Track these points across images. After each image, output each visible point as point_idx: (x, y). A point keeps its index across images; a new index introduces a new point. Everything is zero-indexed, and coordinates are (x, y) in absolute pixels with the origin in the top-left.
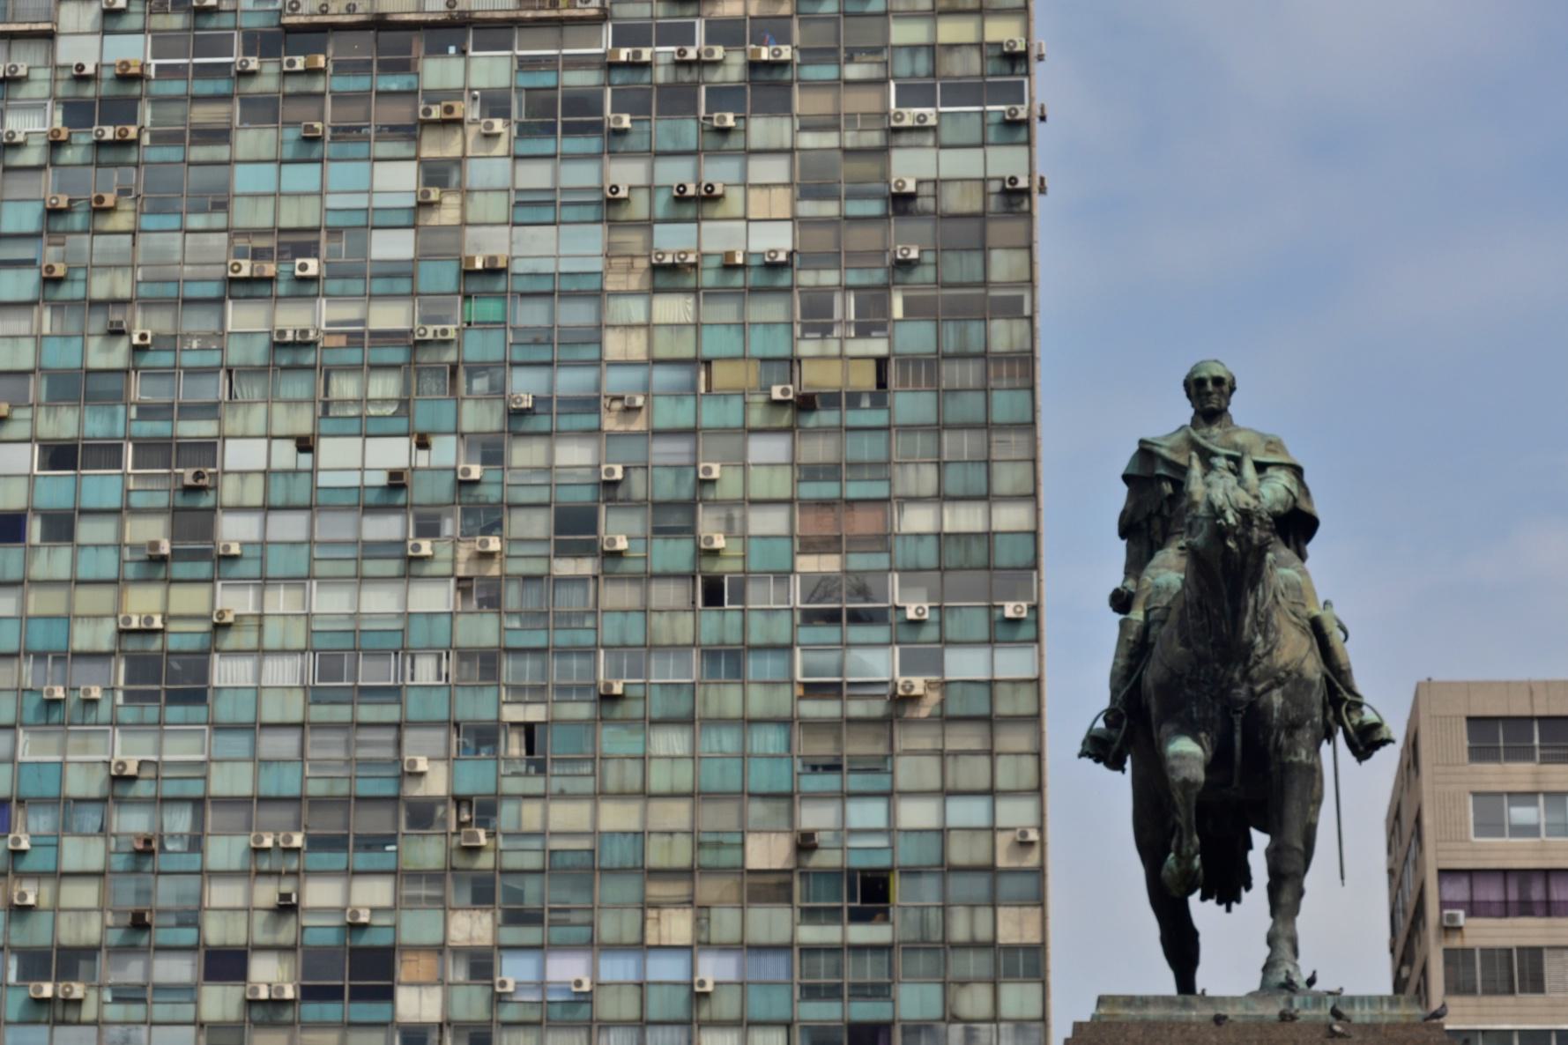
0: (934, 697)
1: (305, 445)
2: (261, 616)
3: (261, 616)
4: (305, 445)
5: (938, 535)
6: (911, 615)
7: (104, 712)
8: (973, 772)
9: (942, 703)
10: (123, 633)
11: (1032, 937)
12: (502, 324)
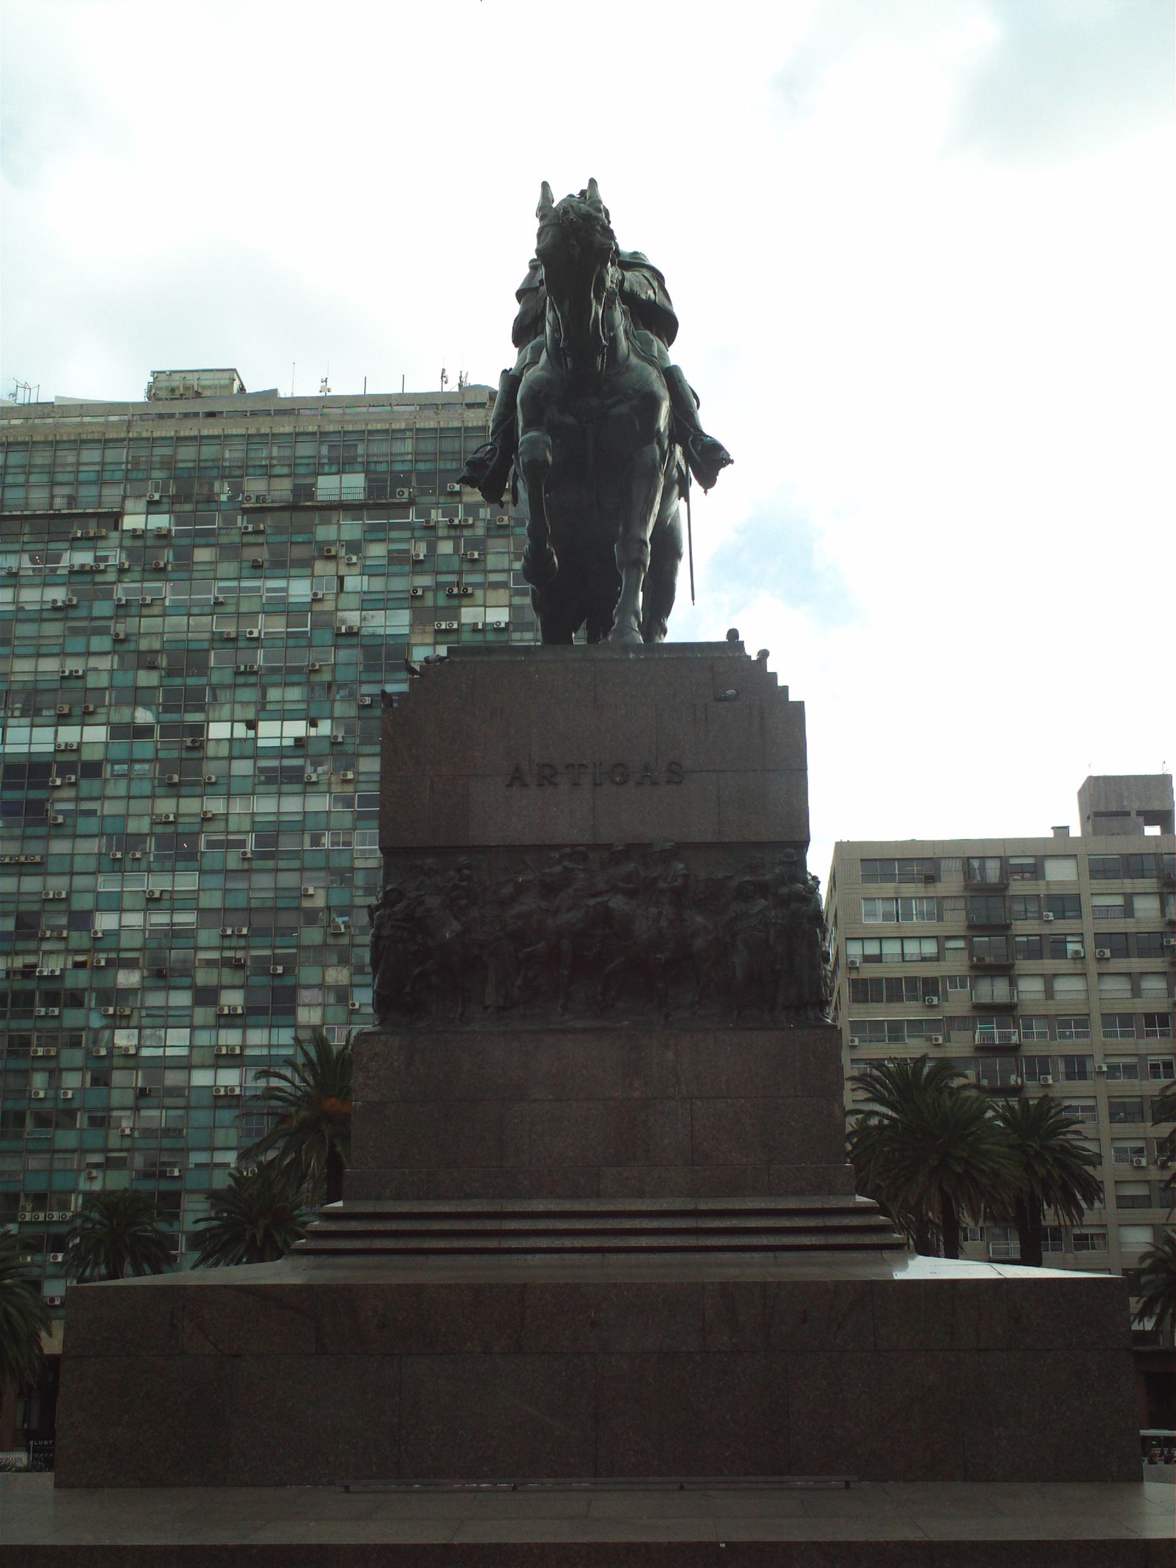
1: (251, 725)
4: (251, 725)
7: (144, 865)
12: (22, 1224)
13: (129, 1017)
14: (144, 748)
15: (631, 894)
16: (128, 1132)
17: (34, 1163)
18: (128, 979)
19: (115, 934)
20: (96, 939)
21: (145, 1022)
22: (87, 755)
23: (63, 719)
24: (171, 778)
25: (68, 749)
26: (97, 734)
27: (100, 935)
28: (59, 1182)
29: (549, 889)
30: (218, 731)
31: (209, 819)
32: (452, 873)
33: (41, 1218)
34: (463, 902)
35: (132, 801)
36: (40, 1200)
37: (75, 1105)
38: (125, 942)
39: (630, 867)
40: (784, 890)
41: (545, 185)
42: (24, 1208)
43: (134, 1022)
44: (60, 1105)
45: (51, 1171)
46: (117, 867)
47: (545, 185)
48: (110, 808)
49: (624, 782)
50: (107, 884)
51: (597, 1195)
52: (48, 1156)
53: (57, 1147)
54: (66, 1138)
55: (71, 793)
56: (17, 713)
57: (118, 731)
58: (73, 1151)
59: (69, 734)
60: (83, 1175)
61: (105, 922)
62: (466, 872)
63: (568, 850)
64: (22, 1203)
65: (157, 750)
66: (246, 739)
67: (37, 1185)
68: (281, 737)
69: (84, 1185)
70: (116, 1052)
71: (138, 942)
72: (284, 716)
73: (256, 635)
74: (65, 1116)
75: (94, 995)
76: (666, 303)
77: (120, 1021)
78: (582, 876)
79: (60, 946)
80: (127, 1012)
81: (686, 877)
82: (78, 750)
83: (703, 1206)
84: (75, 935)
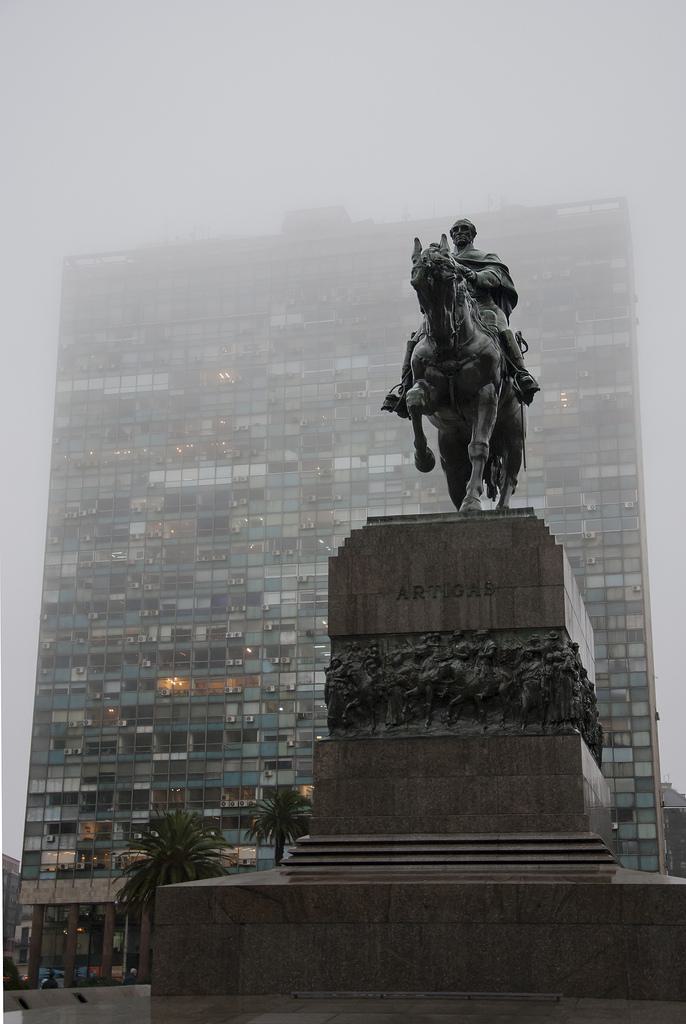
0: (600, 538)
1: (364, 458)
2: (350, 521)
3: (350, 521)
4: (364, 458)
5: (598, 478)
6: (589, 508)
7: (295, 558)
8: (616, 566)
9: (603, 541)
10: (301, 530)
11: (648, 773)
12: (223, 809)
13: (289, 664)
14: (291, 478)
15: (464, 659)
16: (291, 744)
17: (231, 766)
18: (288, 638)
19: (278, 607)
20: (265, 611)
21: (300, 667)
22: (254, 484)
23: (236, 460)
24: (311, 498)
25: (241, 481)
26: (260, 469)
27: (267, 608)
28: (248, 780)
29: (419, 658)
30: (341, 464)
31: (339, 525)
32: (367, 649)
33: (236, 805)
34: (372, 666)
35: (286, 515)
36: (235, 792)
37: (256, 726)
38: (285, 613)
39: (462, 644)
40: (549, 655)
41: (417, 240)
42: (224, 798)
43: (293, 668)
44: (245, 727)
45: (241, 772)
46: (277, 560)
47: (417, 240)
48: (274, 520)
49: (461, 595)
50: (272, 573)
51: (446, 832)
52: (239, 761)
53: (245, 755)
54: (251, 749)
55: (244, 511)
56: (204, 458)
57: (274, 467)
58: (256, 758)
59: (241, 471)
60: (263, 775)
61: (271, 599)
62: (375, 649)
63: (430, 635)
64: (223, 794)
65: (301, 479)
66: (360, 469)
67: (234, 782)
68: (385, 466)
69: (263, 782)
70: (281, 689)
71: (293, 613)
72: (386, 451)
73: (364, 395)
74: (248, 735)
75: (265, 650)
76: (510, 285)
77: (282, 668)
78: (436, 650)
79: (242, 617)
80: (288, 661)
81: (495, 649)
82: (248, 482)
83: (503, 837)
84: (251, 608)
